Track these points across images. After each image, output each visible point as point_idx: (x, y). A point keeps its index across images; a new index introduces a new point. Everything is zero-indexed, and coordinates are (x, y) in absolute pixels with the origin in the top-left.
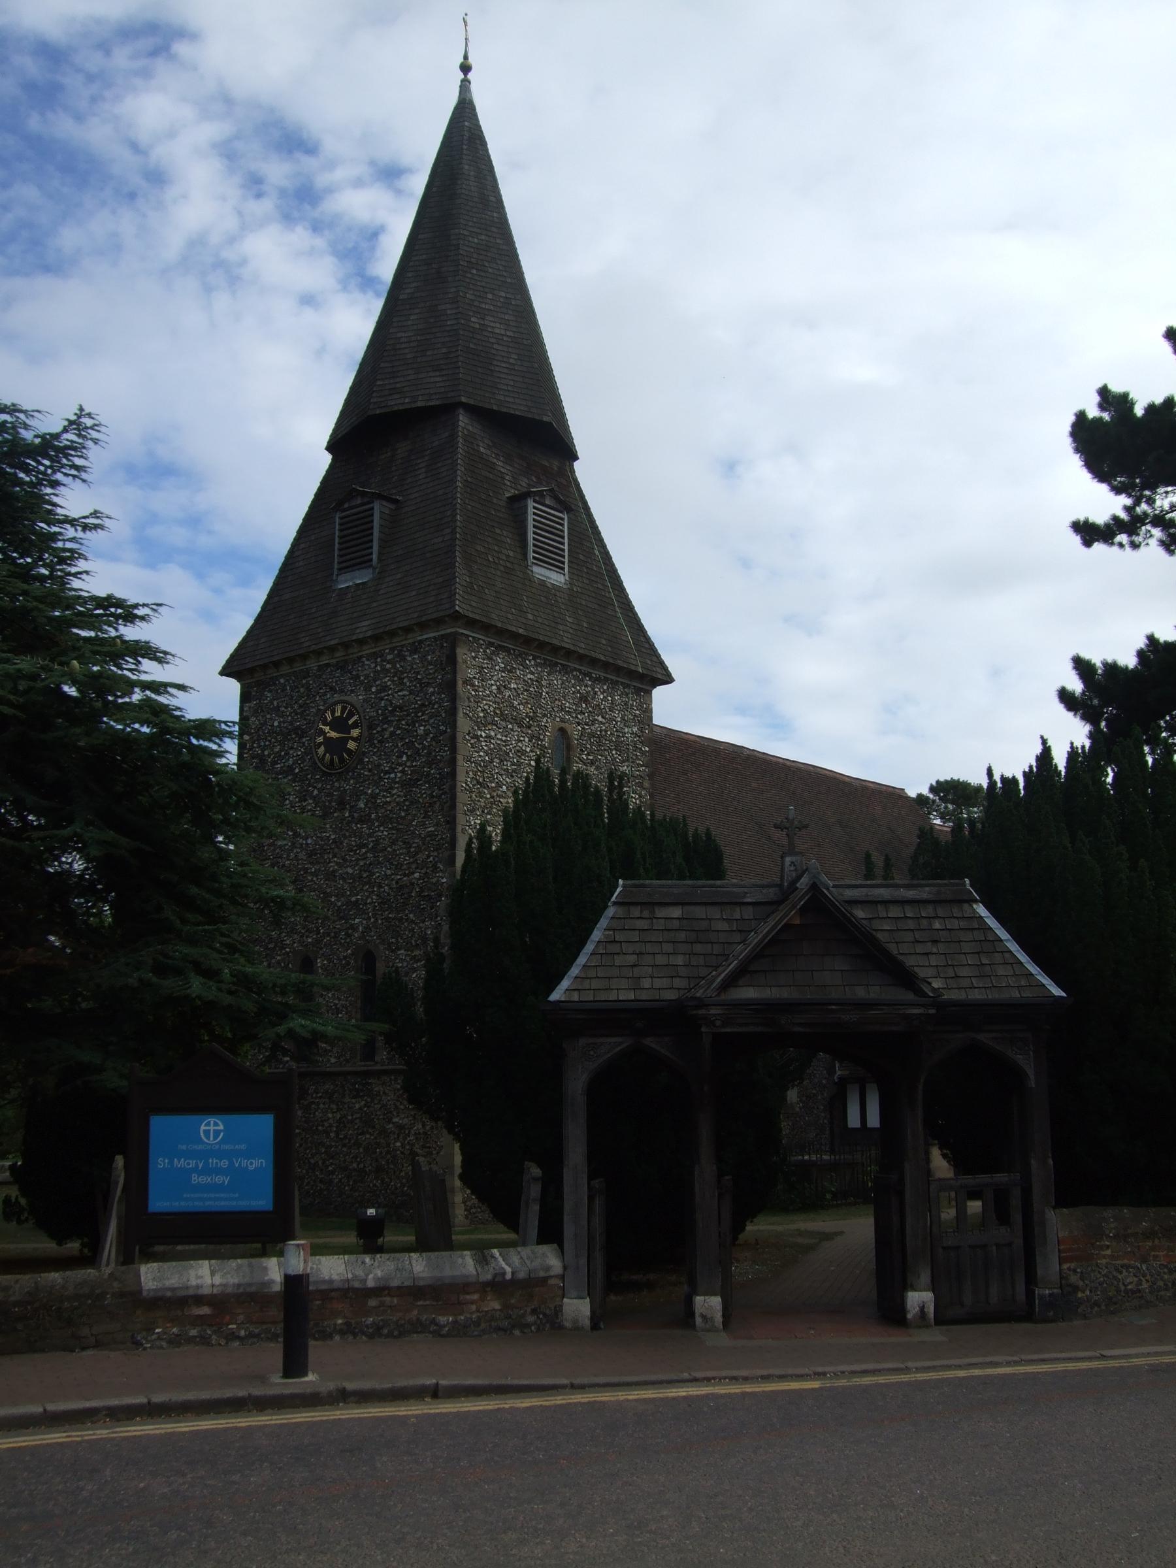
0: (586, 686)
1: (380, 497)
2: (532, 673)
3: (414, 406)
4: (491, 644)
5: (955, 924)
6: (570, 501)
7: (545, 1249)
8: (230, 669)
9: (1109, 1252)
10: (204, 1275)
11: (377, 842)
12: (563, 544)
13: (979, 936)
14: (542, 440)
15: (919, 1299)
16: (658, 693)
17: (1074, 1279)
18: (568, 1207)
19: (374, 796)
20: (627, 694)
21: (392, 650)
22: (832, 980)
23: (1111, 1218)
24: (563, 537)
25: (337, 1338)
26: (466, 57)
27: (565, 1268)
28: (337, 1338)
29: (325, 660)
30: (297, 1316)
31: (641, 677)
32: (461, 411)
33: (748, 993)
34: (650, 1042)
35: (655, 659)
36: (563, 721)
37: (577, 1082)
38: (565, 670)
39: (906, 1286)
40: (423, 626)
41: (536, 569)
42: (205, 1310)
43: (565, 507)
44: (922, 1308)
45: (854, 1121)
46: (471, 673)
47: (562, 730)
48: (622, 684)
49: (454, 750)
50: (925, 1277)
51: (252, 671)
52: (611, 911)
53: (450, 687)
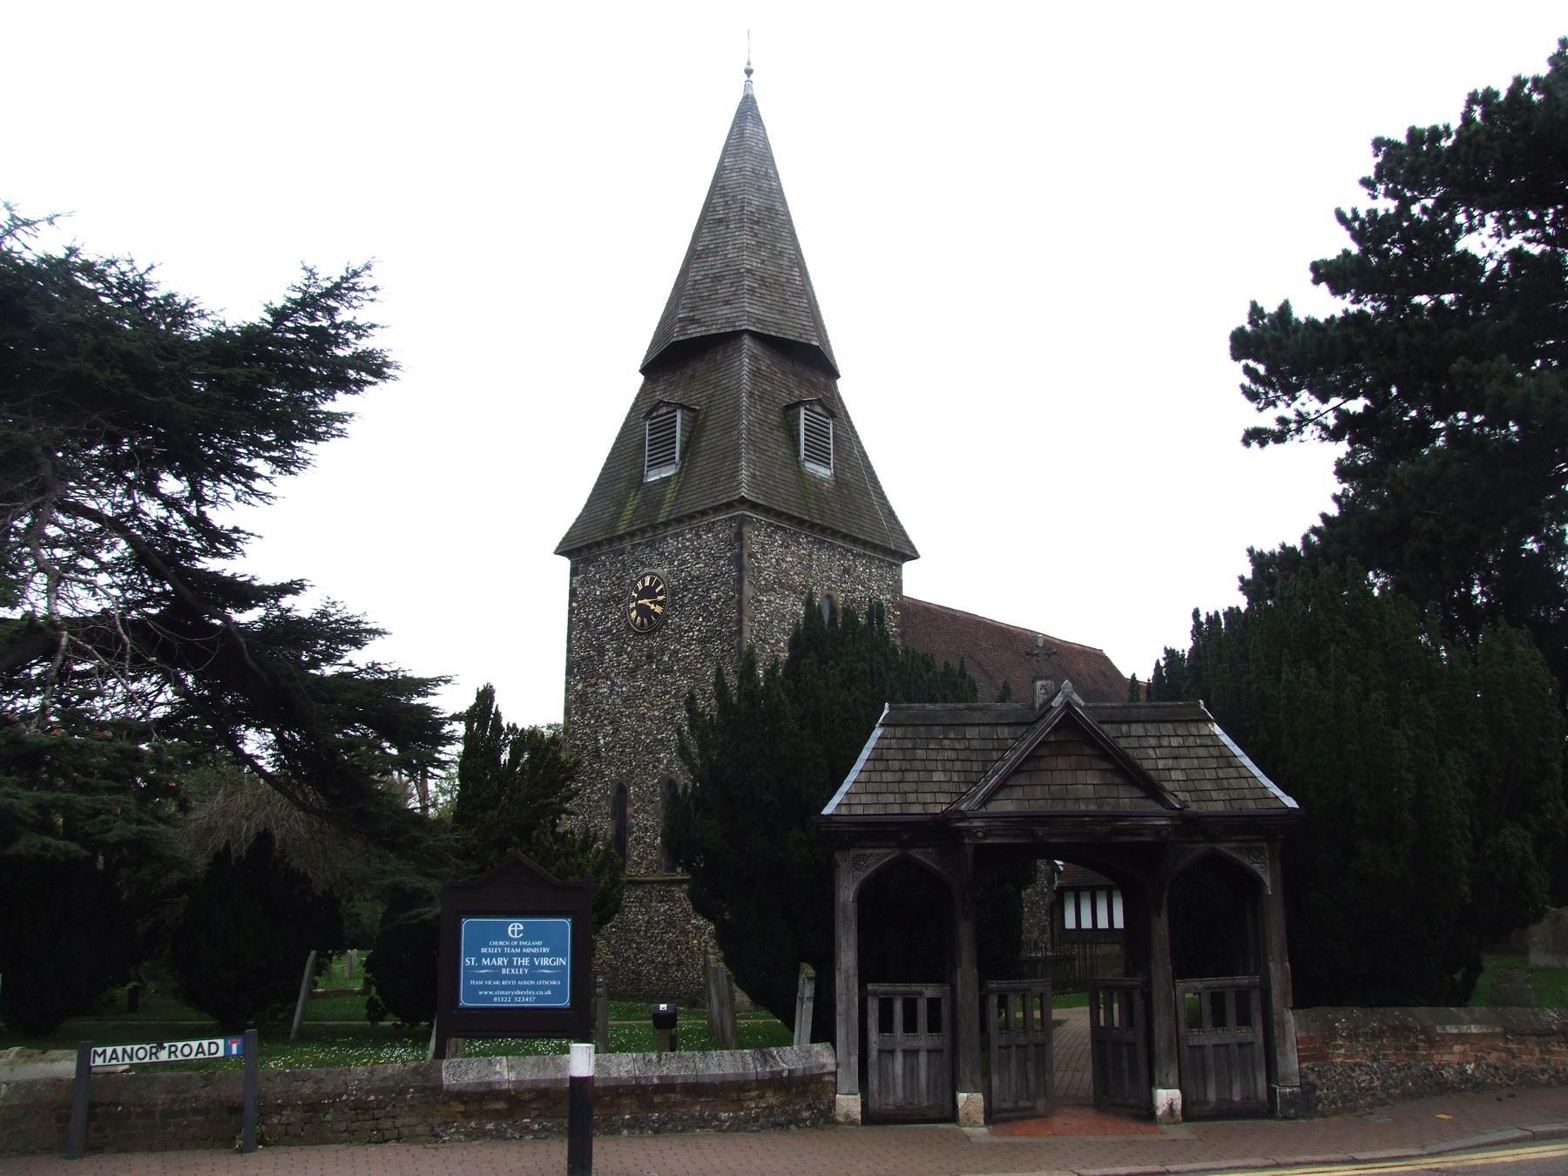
5: (1191, 741)
6: (833, 409)
7: (817, 1047)
8: (562, 550)
9: (1342, 1051)
10: (505, 1071)
11: (678, 690)
13: (1215, 752)
14: (813, 362)
16: (907, 567)
17: (1312, 1077)
18: (840, 1008)
19: (676, 652)
23: (1342, 1020)
25: (625, 1132)
27: (837, 1065)
28: (625, 1132)
30: (581, 1113)
31: (894, 553)
34: (917, 853)
36: (830, 588)
37: (847, 893)
38: (832, 546)
39: (1152, 1084)
40: (717, 510)
41: (807, 464)
42: (500, 1105)
43: (833, 415)
44: (1171, 1106)
45: (1070, 923)
46: (756, 548)
49: (741, 612)
50: (1173, 1078)
51: (579, 550)
52: (878, 732)
53: (738, 560)
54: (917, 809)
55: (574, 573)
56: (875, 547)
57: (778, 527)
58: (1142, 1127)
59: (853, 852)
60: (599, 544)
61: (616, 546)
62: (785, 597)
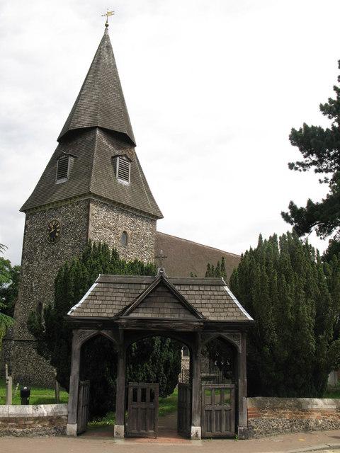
6: (133, 159)
14: (125, 140)
15: (196, 429)
16: (158, 221)
17: (252, 424)
19: (63, 251)
22: (165, 313)
27: (69, 412)
33: (133, 315)
37: (76, 346)
38: (127, 212)
40: (80, 196)
47: (125, 232)
52: (95, 285)
54: (105, 315)
55: (27, 219)
58: (186, 441)
59: (80, 331)
62: (106, 231)
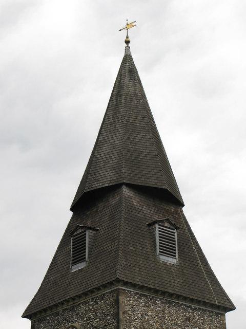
0: (189, 313)
1: (89, 228)
2: (160, 307)
3: (104, 186)
4: (137, 293)
12: (175, 244)
14: (167, 197)
16: (228, 315)
20: (211, 316)
21: (93, 299)
24: (175, 241)
26: (127, 37)
29: (65, 307)
31: (218, 307)
32: (124, 187)
35: (225, 298)
40: (105, 286)
46: (127, 308)
48: (208, 311)
51: (35, 314)
53: (116, 315)
56: (205, 304)
57: (142, 295)
60: (45, 310)
61: (54, 311)
